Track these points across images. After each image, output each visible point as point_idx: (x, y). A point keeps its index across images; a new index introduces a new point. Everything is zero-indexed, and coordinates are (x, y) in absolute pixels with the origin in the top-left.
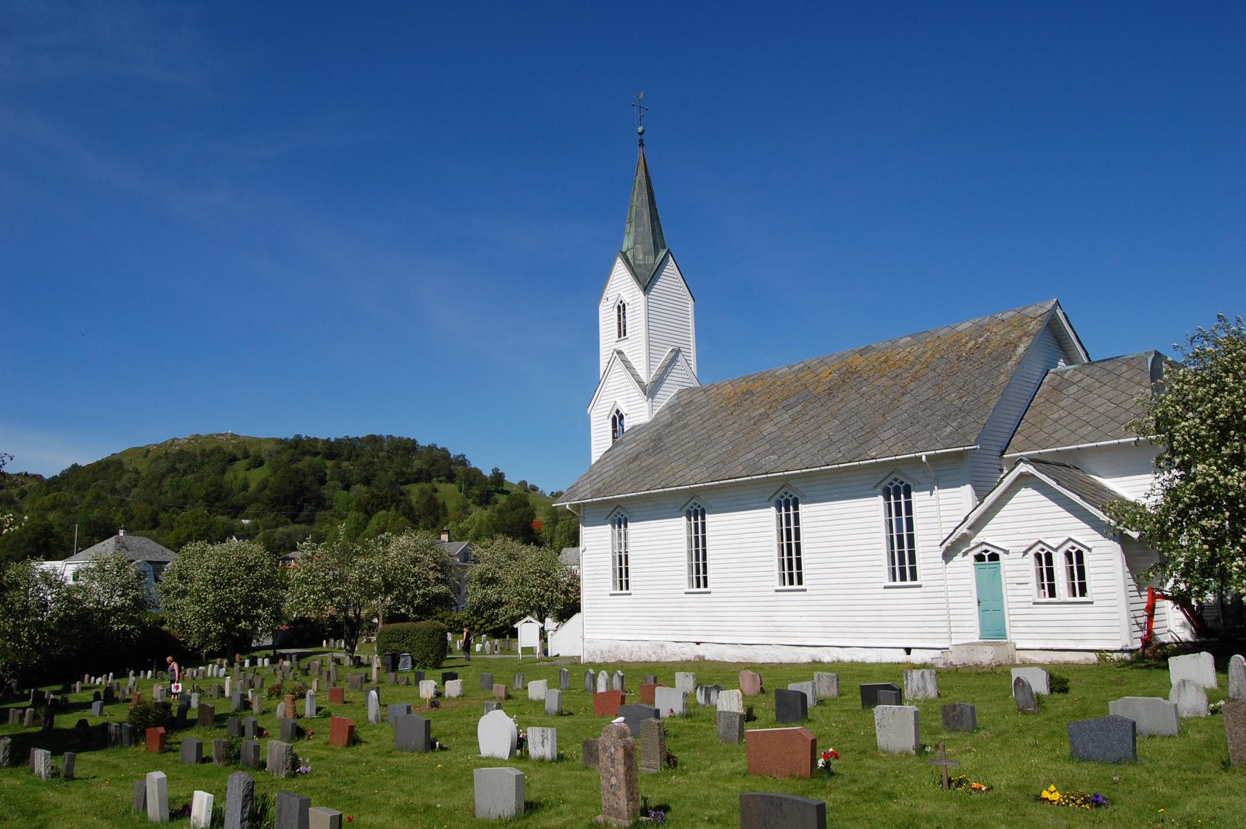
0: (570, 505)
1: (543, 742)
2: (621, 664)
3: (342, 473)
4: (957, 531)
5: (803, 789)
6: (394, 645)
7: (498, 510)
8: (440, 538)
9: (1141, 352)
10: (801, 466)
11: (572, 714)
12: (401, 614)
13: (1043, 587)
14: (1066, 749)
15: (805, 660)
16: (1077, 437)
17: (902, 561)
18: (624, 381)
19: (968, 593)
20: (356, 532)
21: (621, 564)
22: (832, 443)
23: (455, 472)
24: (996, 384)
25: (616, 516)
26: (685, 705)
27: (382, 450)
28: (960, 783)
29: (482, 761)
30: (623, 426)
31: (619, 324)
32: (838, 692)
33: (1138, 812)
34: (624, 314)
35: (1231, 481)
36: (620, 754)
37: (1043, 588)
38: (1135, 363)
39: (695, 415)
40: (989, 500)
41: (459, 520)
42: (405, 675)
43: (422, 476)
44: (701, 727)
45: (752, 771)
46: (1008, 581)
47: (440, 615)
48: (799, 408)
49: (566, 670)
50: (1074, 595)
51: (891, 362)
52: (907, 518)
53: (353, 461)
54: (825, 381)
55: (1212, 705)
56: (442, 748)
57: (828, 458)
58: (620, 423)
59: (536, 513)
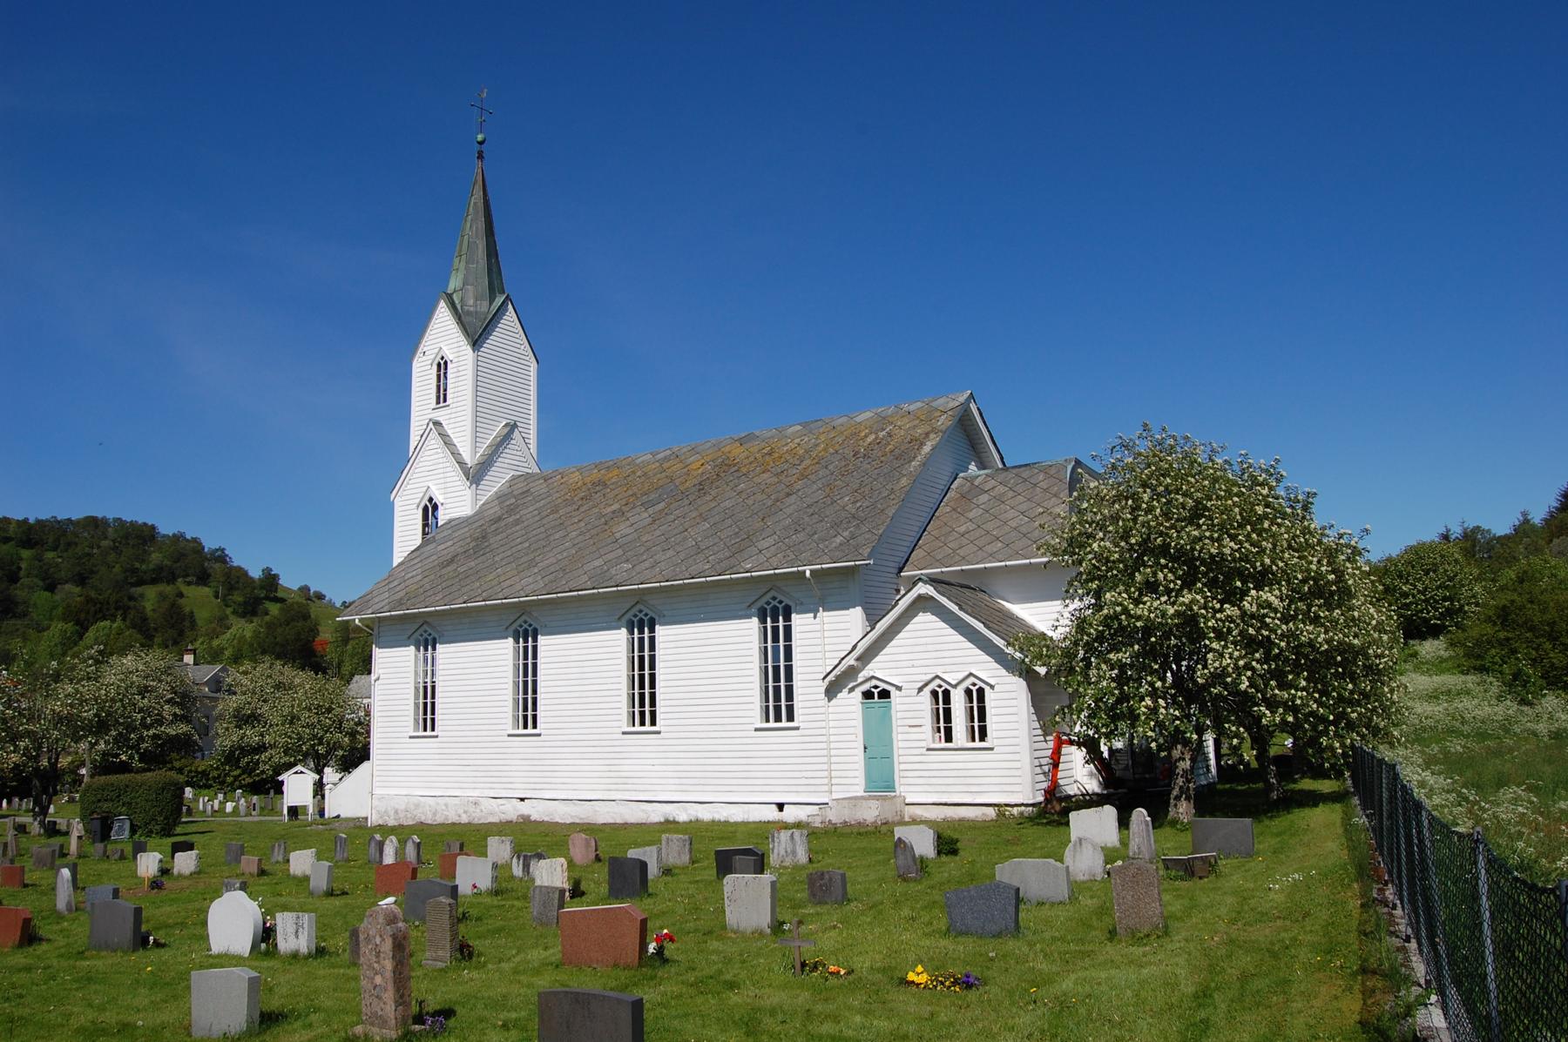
0: (360, 620)
1: (297, 932)
2: (420, 828)
3: (45, 567)
4: (843, 662)
5: (628, 981)
6: (106, 806)
7: (267, 623)
8: (182, 660)
9: (1061, 460)
10: (659, 578)
11: (347, 894)
12: (122, 762)
13: (939, 730)
14: (943, 924)
15: (656, 819)
16: (985, 555)
17: (777, 698)
18: (441, 460)
19: (853, 737)
20: (69, 644)
21: (425, 697)
22: (699, 551)
23: (210, 571)
24: (895, 488)
25: (421, 635)
26: (495, 879)
27: (106, 538)
28: (815, 968)
29: (211, 960)
30: (437, 519)
31: (438, 387)
32: (691, 858)
33: (1011, 993)
34: (445, 373)
35: (1141, 610)
36: (387, 946)
37: (939, 731)
38: (1053, 471)
39: (531, 509)
40: (882, 625)
41: (214, 634)
42: (119, 847)
43: (162, 575)
44: (513, 906)
45: (569, 960)
46: (900, 722)
47: (177, 764)
48: (662, 505)
49: (344, 836)
50: (973, 740)
51: (776, 455)
52: (785, 646)
53: (61, 551)
54: (695, 473)
55: (1109, 866)
56: (157, 944)
57: (694, 569)
58: (433, 514)
59: (320, 629)
